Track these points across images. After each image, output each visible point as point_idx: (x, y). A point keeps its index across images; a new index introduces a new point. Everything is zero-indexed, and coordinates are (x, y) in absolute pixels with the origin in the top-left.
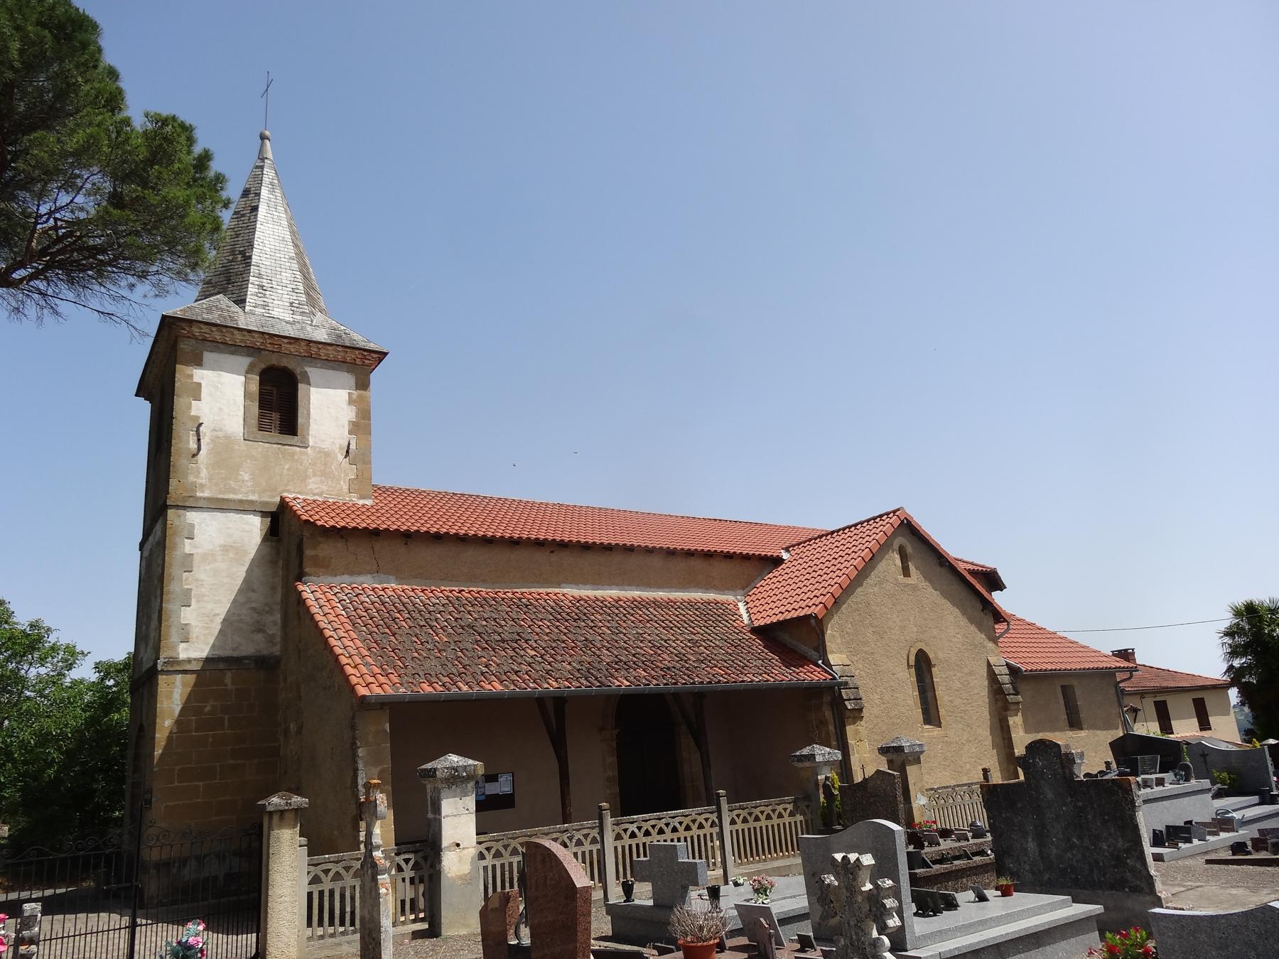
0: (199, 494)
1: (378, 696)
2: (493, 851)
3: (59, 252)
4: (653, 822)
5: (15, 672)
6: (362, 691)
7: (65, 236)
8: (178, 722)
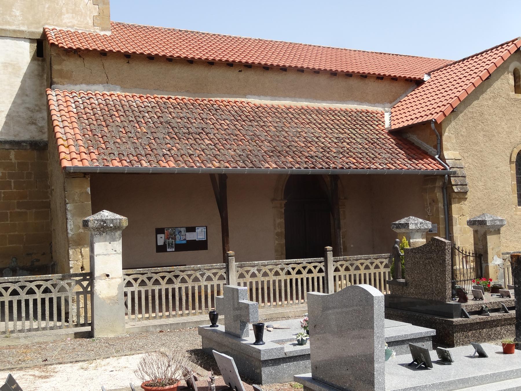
2: (139, 281)
4: (270, 267)
6: (66, 163)
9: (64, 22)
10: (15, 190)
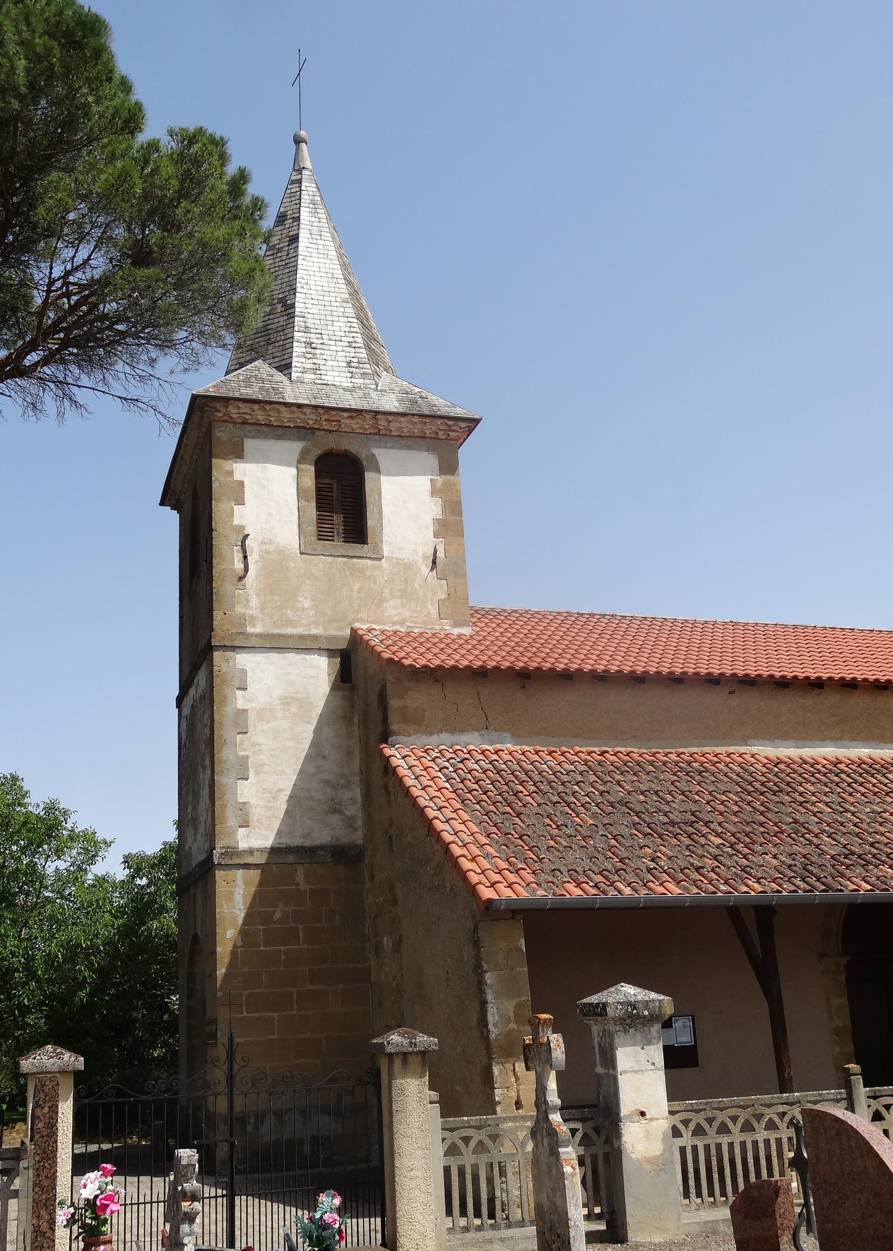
0: (250, 630)
1: (509, 900)
2: (692, 1126)
3: (77, 325)
5: (32, 866)
6: (487, 893)
7: (78, 304)
8: (243, 933)
9: (386, 614)
10: (305, 946)
